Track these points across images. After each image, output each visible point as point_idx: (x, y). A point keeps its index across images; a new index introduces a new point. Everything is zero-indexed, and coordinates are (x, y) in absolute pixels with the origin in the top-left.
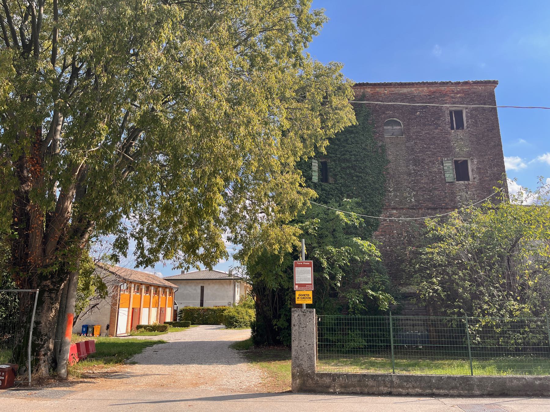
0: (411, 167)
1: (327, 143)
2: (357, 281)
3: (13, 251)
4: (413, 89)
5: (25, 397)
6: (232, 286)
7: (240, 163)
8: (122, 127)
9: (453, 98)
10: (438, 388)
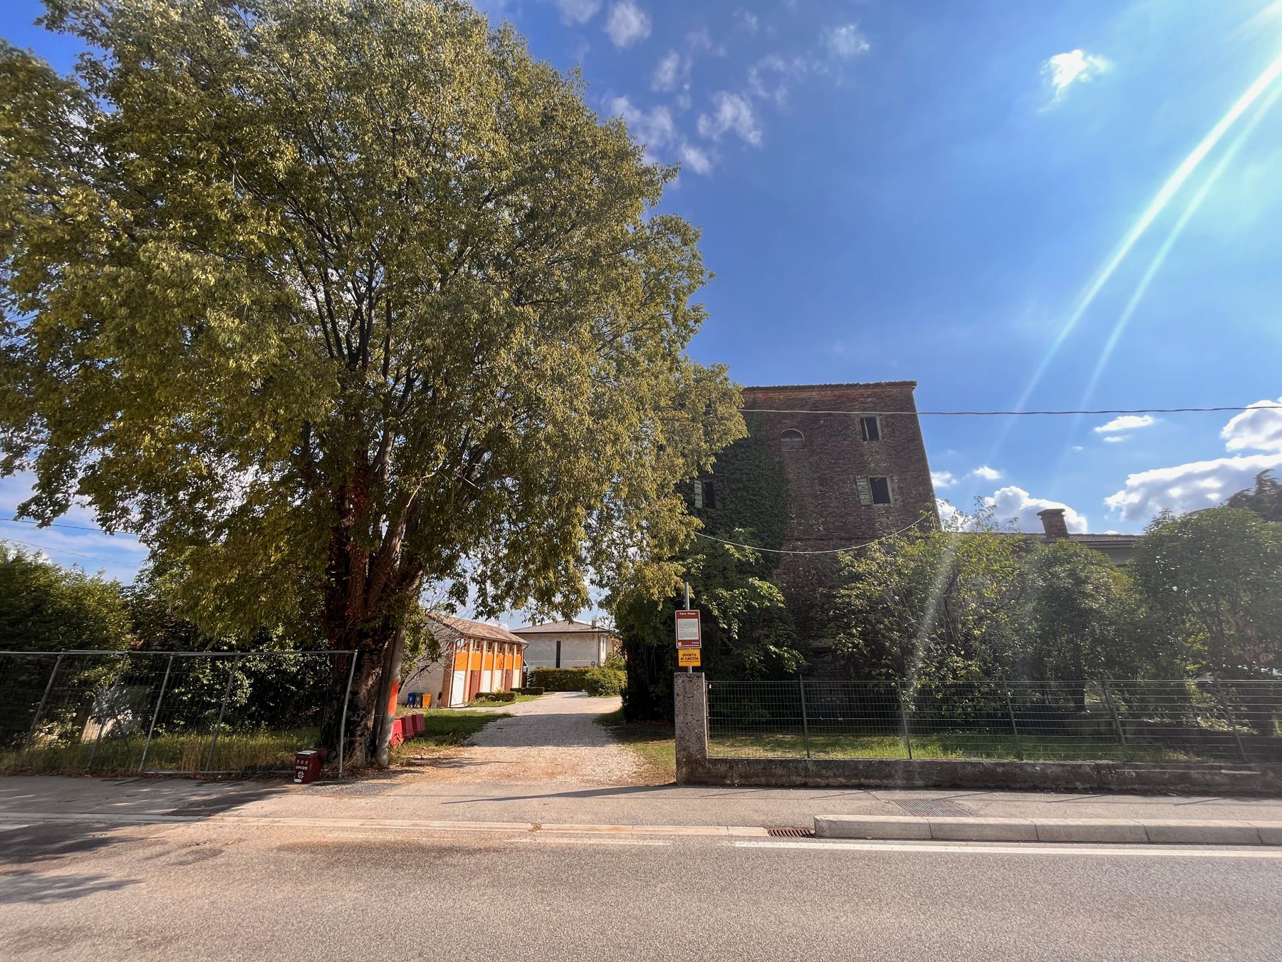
1: (713, 459)
2: (756, 634)
3: (328, 601)
5: (334, 794)
6: (596, 641)
7: (606, 488)
8: (463, 447)
10: (867, 778)
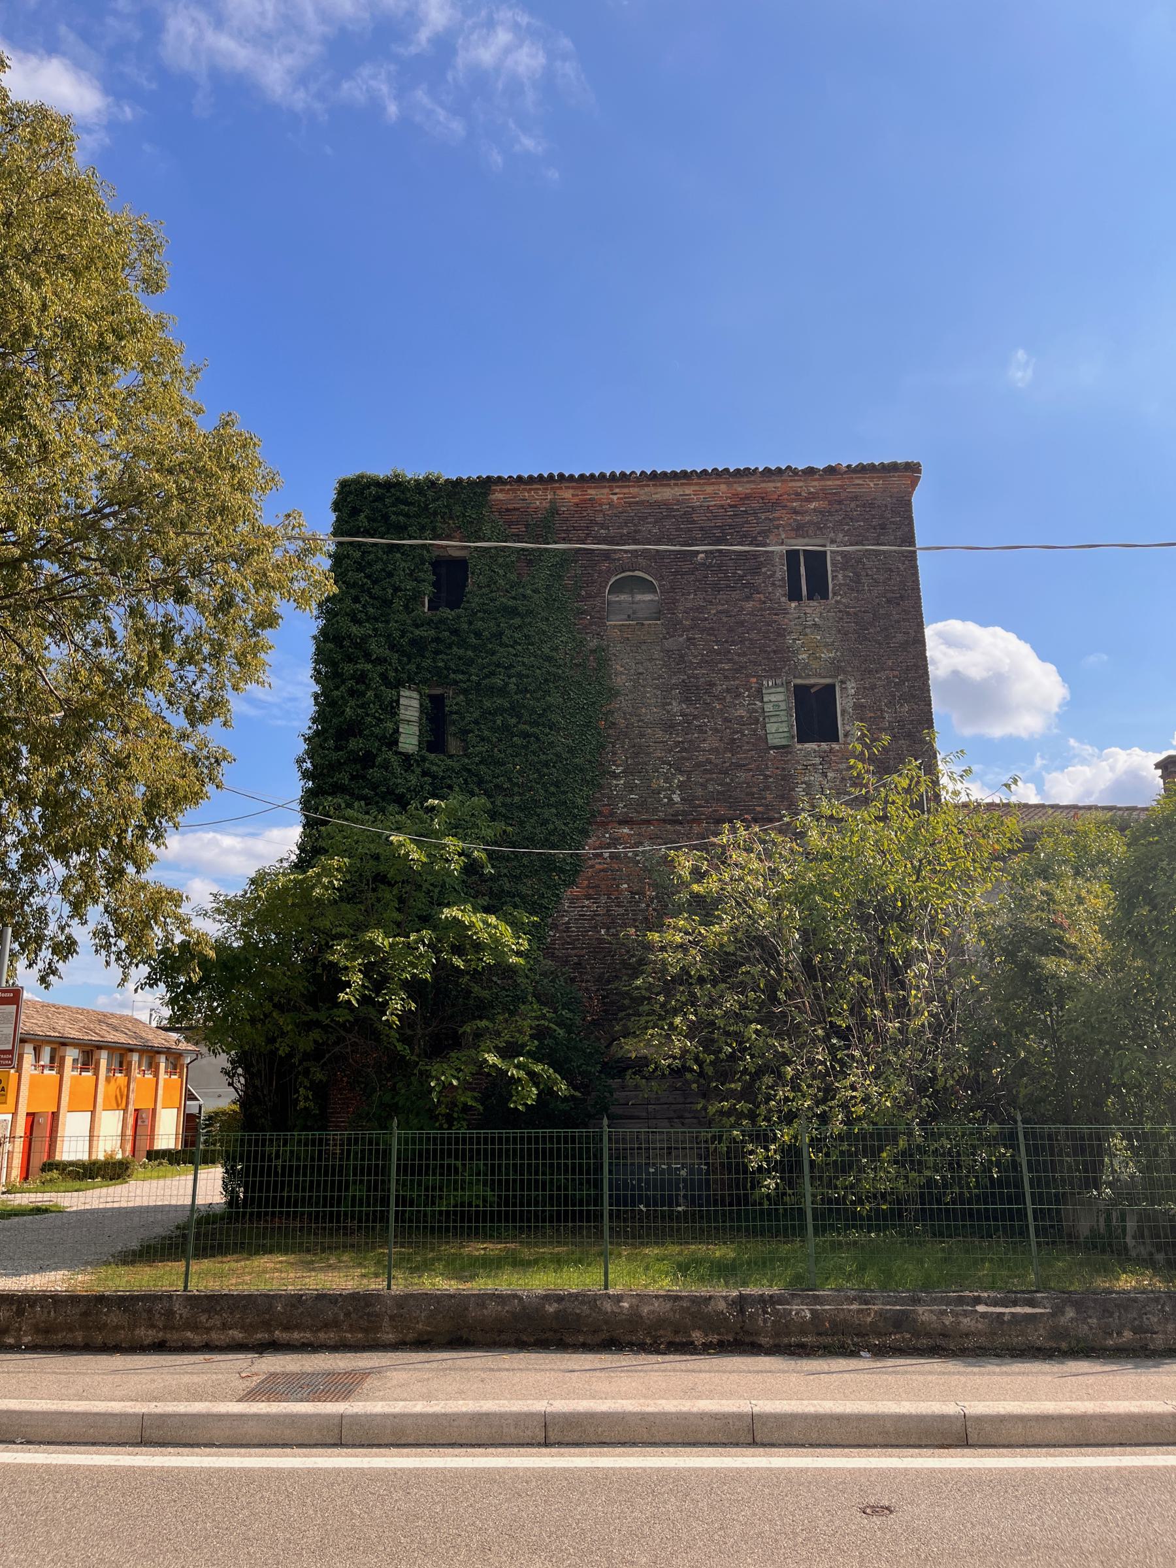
0: (675, 707)
4: (688, 490)
9: (796, 512)
10: (287, 1328)
